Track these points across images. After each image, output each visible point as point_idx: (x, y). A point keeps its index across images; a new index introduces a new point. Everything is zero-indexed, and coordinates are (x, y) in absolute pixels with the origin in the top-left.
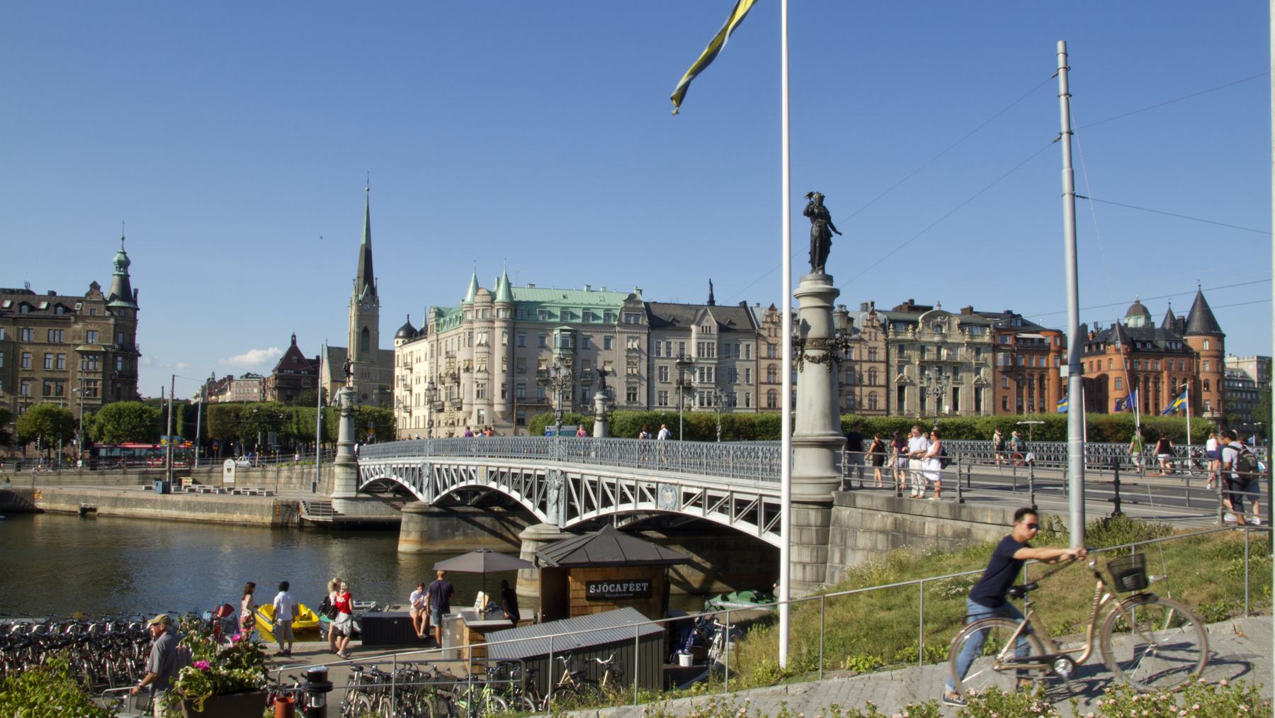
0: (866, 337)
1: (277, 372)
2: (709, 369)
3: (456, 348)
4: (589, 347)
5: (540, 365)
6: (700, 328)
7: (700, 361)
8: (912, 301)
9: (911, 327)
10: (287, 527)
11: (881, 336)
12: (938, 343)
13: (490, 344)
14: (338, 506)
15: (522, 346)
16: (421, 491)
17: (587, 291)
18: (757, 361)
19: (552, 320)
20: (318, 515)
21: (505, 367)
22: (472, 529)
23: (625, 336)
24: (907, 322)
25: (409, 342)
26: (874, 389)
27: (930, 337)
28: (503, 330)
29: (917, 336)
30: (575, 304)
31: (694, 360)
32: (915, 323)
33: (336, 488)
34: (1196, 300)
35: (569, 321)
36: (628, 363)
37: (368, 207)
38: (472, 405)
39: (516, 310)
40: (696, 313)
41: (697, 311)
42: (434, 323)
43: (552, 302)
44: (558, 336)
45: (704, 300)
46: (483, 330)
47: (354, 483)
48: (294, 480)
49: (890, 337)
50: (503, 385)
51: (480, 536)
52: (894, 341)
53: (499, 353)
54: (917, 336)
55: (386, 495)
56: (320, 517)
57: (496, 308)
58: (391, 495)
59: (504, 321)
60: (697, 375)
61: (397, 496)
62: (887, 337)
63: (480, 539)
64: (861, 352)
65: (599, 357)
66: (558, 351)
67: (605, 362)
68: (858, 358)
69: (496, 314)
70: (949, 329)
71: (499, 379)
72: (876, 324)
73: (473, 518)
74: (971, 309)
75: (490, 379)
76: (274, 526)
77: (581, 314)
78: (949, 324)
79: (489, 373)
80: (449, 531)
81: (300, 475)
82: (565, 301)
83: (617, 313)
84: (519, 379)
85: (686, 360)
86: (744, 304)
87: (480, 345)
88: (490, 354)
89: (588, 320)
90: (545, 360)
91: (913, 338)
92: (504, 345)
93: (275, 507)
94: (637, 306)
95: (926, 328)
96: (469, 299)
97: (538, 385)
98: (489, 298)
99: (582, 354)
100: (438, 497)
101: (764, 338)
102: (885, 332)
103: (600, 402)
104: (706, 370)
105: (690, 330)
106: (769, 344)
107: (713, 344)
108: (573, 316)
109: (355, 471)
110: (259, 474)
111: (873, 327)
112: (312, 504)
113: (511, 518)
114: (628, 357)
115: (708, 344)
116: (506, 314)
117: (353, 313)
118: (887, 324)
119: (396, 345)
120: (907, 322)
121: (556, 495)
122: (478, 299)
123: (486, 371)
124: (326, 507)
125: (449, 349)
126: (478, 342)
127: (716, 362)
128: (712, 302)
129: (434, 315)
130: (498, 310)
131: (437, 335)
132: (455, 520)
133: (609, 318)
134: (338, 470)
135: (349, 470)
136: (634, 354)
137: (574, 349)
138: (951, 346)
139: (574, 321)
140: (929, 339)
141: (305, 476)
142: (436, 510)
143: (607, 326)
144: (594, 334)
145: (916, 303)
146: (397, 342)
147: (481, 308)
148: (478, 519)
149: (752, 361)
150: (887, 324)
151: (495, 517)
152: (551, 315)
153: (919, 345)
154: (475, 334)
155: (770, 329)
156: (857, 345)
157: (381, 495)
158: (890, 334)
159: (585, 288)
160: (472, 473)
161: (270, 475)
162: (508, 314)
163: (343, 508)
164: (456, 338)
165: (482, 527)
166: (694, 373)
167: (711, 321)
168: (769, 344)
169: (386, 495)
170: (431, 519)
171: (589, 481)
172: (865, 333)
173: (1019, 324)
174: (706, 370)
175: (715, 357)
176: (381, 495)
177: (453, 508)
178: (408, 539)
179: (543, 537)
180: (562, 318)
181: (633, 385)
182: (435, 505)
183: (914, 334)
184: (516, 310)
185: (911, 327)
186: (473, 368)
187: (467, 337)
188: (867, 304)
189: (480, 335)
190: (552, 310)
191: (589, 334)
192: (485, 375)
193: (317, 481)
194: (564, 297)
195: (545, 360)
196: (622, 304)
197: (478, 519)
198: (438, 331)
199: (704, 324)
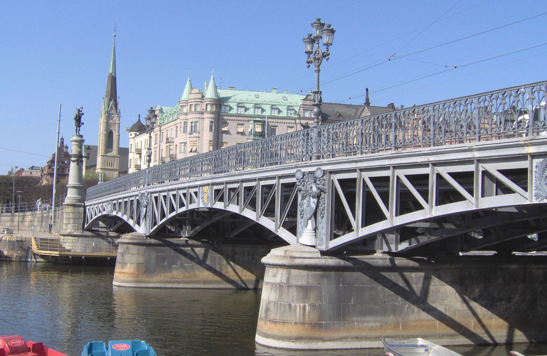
1: (50, 163)
3: (173, 135)
16: (139, 223)
20: (47, 250)
25: (140, 134)
37: (114, 47)
40: (357, 111)
41: (357, 110)
48: (36, 224)
69: (205, 108)
86: (392, 106)
98: (200, 96)
100: (156, 227)
110: (8, 218)
112: (41, 239)
117: (102, 120)
119: (130, 137)
121: (313, 206)
125: (169, 136)
128: (367, 103)
141: (44, 220)
142: (153, 241)
146: (131, 135)
147: (194, 103)
160: (193, 195)
161: (16, 219)
164: (174, 128)
171: (371, 178)
178: (123, 271)
179: (298, 262)
182: (150, 236)
184: (220, 105)
187: (183, 125)
193: (53, 223)
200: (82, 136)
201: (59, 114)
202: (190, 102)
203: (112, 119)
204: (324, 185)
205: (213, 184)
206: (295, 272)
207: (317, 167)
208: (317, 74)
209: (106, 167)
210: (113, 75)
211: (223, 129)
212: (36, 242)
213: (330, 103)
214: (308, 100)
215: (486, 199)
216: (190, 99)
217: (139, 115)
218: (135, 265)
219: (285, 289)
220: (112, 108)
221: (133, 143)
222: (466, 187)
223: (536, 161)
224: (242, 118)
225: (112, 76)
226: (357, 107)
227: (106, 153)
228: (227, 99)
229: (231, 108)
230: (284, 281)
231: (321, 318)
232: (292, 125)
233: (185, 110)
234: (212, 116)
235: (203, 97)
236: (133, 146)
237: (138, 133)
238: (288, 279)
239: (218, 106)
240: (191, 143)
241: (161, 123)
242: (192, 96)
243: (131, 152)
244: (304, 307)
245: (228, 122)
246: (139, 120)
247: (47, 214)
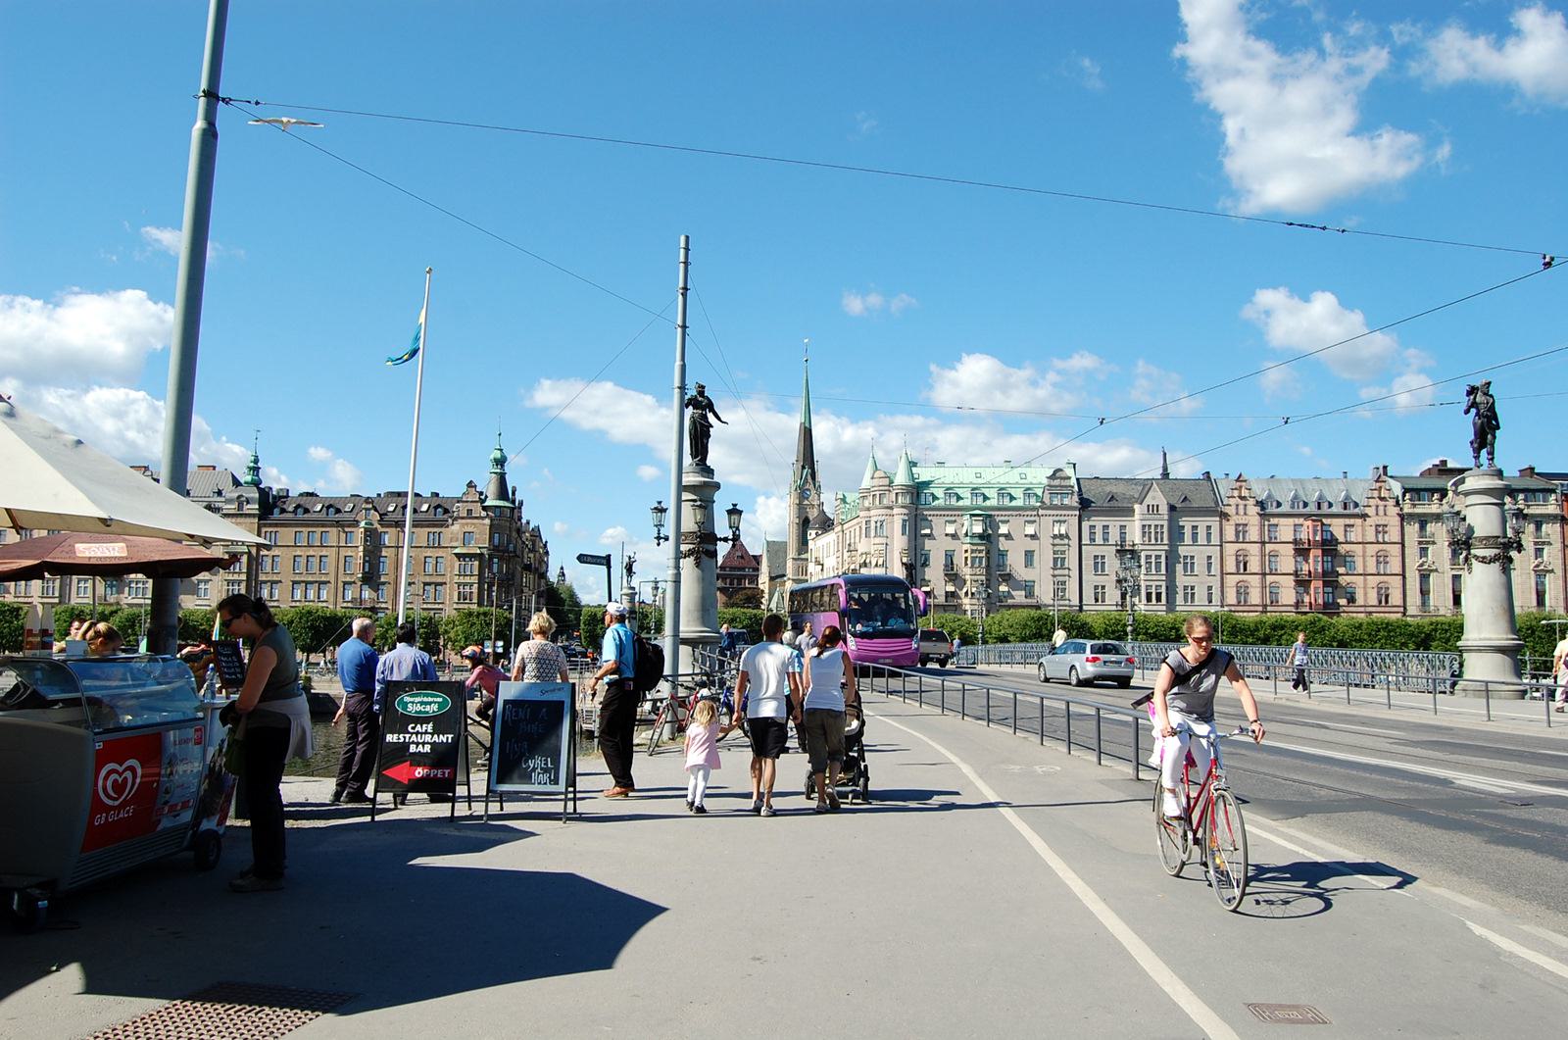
2: (1158, 557)
18: (1221, 546)
26: (1384, 546)
37: (807, 380)
52: (1411, 515)
69: (894, 499)
107: (1162, 526)
127: (1166, 548)
128: (1165, 475)
145: (1450, 465)
147: (878, 493)
203: (807, 499)
209: (800, 577)
210: (807, 425)
211: (923, 532)
214: (1057, 479)
220: (806, 479)
224: (953, 512)
225: (805, 428)
227: (799, 555)
228: (927, 484)
229: (935, 498)
232: (1032, 518)
233: (867, 504)
234: (905, 511)
235: (891, 482)
237: (820, 532)
241: (843, 520)
242: (876, 482)
245: (929, 518)
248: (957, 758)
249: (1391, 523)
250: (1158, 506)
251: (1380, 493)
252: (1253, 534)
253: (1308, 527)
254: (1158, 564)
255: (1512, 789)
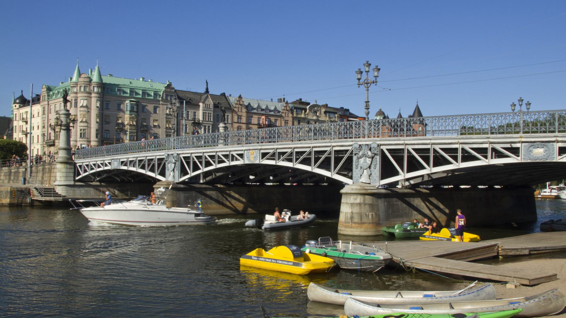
0: (283, 115)
2: (209, 127)
4: (145, 111)
5: (118, 120)
6: (205, 105)
7: (204, 122)
8: (301, 99)
9: (303, 111)
10: (21, 206)
11: (290, 115)
12: (315, 120)
13: (89, 107)
14: (60, 190)
15: (107, 108)
17: (143, 80)
18: (232, 124)
19: (125, 95)
20: (51, 196)
21: (98, 120)
22: (205, 199)
23: (165, 106)
24: (302, 109)
25: (24, 106)
27: (312, 117)
28: (97, 98)
29: (306, 116)
30: (137, 87)
31: (201, 122)
32: (305, 110)
33: (58, 178)
34: (416, 108)
35: (134, 96)
36: (167, 122)
38: (77, 141)
39: (104, 88)
42: (46, 94)
43: (124, 85)
44: (129, 104)
45: (203, 90)
46: (84, 98)
47: (72, 175)
49: (294, 116)
50: (97, 130)
51: (210, 204)
52: (296, 118)
53: (94, 112)
54: (306, 116)
55: (94, 183)
56: (52, 198)
57: (92, 85)
58: (98, 184)
59: (98, 93)
60: (203, 129)
61: (102, 184)
62: (293, 115)
63: (210, 206)
64: (281, 122)
65: (151, 117)
66: (128, 112)
67: (154, 120)
68: (280, 125)
69: (92, 89)
70: (320, 114)
71: (94, 126)
72: (288, 109)
73: (205, 192)
74: (327, 105)
75: (89, 127)
76: (11, 205)
77: (141, 93)
78: (320, 111)
79: (88, 123)
80: (190, 201)
81: (8, 174)
82: (131, 85)
83: (161, 94)
84: (106, 127)
85: (196, 121)
86: (223, 95)
87: (82, 107)
88: (89, 112)
89: (145, 96)
90: (121, 117)
91: (304, 117)
92: (97, 107)
93: (11, 192)
94: (171, 91)
95: (310, 112)
96: (74, 79)
97: (117, 131)
98: (88, 80)
99: (142, 116)
101: (236, 113)
102: (292, 113)
103: (223, 128)
104: (207, 127)
105: (199, 106)
106: (238, 115)
107: (211, 113)
108: (137, 94)
109: (72, 167)
111: (287, 110)
113: (228, 192)
114: (166, 118)
115: (209, 113)
116: (99, 90)
118: (293, 109)
119: (14, 108)
120: (302, 109)
122: (81, 80)
123: (86, 122)
124: (50, 191)
126: (81, 105)
127: (212, 123)
128: (207, 91)
129: (45, 89)
130: (94, 87)
131: (48, 102)
132: (194, 193)
133: (157, 96)
134: (59, 166)
135: (68, 166)
136: (170, 117)
137: (137, 112)
138: (321, 122)
139: (137, 96)
140: (312, 118)
141: (13, 174)
143: (155, 101)
144: (148, 105)
145: (303, 100)
146: (15, 106)
147: (83, 85)
148: (208, 193)
149: (230, 124)
150: (293, 109)
151: (218, 191)
152: (125, 92)
153: (306, 121)
154: (79, 100)
155: (239, 108)
156: (279, 119)
157: (92, 183)
158: (295, 114)
159: (141, 79)
162: (100, 89)
163: (65, 192)
165: (211, 198)
166: (201, 128)
167: (210, 102)
168: (238, 115)
169: (94, 183)
170: (178, 192)
172: (283, 113)
173: (348, 114)
174: (207, 127)
175: (212, 120)
176: (92, 183)
177: (192, 185)
179: (369, 191)
180: (130, 94)
181: (169, 134)
183: (305, 115)
184: (104, 88)
185: (303, 111)
186: (77, 120)
188: (281, 99)
189: (82, 101)
190: (124, 89)
191: (145, 104)
192: (86, 124)
194: (131, 83)
195: (121, 117)
196: (164, 89)
197: (208, 193)
198: (48, 99)
199: (207, 102)
200: (68, 111)
201: (31, 92)
202: (80, 84)
204: (377, 151)
205: (260, 149)
206: (367, 197)
207: (373, 142)
208: (367, 92)
212: (37, 191)
213: (182, 91)
215: (233, 162)
216: (80, 82)
217: (22, 91)
218: (171, 202)
219: (363, 206)
221: (17, 113)
222: (392, 154)
223: (523, 144)
226: (201, 95)
230: (362, 202)
231: (379, 220)
236: (17, 115)
237: (22, 105)
238: (364, 200)
239: (103, 88)
240: (82, 115)
243: (16, 120)
244: (373, 214)
246: (22, 94)
247: (16, 170)
248: (226, 203)
249: (243, 115)
250: (209, 104)
251: (287, 108)
252: (244, 120)
253: (263, 119)
254: (209, 130)
255: (444, 172)
